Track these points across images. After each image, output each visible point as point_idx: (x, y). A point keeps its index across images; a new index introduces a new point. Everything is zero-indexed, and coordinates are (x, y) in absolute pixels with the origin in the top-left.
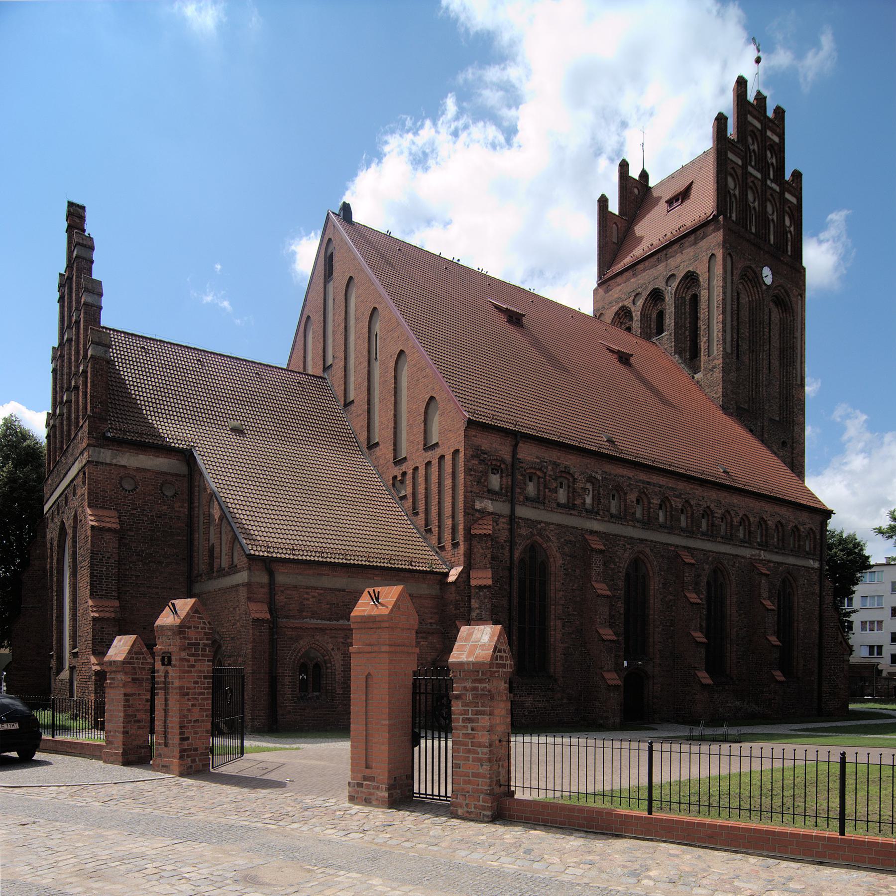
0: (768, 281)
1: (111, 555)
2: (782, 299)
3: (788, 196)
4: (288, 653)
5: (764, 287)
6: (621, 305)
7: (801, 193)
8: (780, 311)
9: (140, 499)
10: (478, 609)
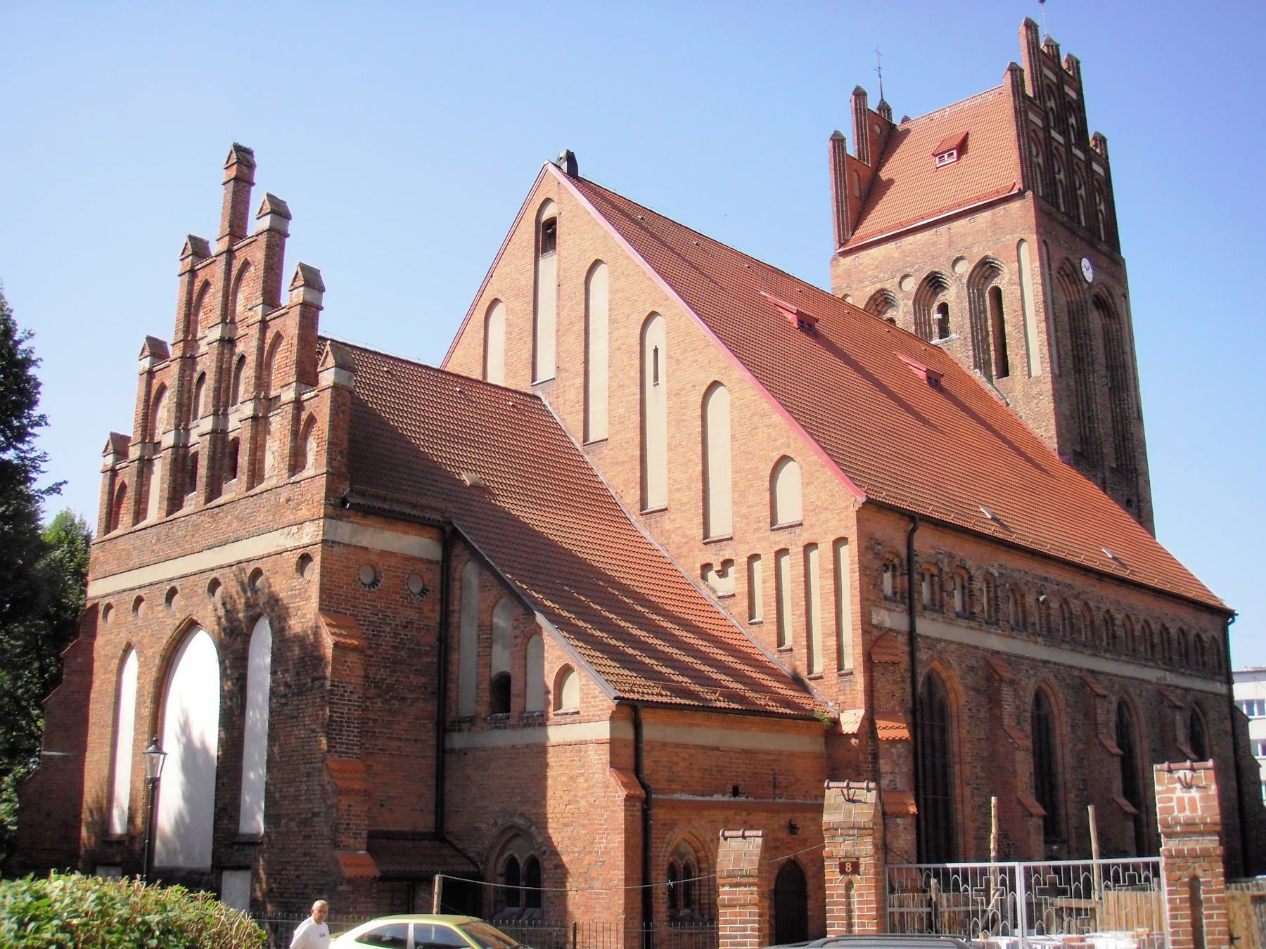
0: (1089, 275)
1: (355, 688)
2: (1104, 300)
3: (1095, 167)
4: (662, 847)
5: (1086, 286)
6: (879, 286)
7: (1108, 163)
8: (1102, 316)
9: (382, 598)
10: (891, 773)
